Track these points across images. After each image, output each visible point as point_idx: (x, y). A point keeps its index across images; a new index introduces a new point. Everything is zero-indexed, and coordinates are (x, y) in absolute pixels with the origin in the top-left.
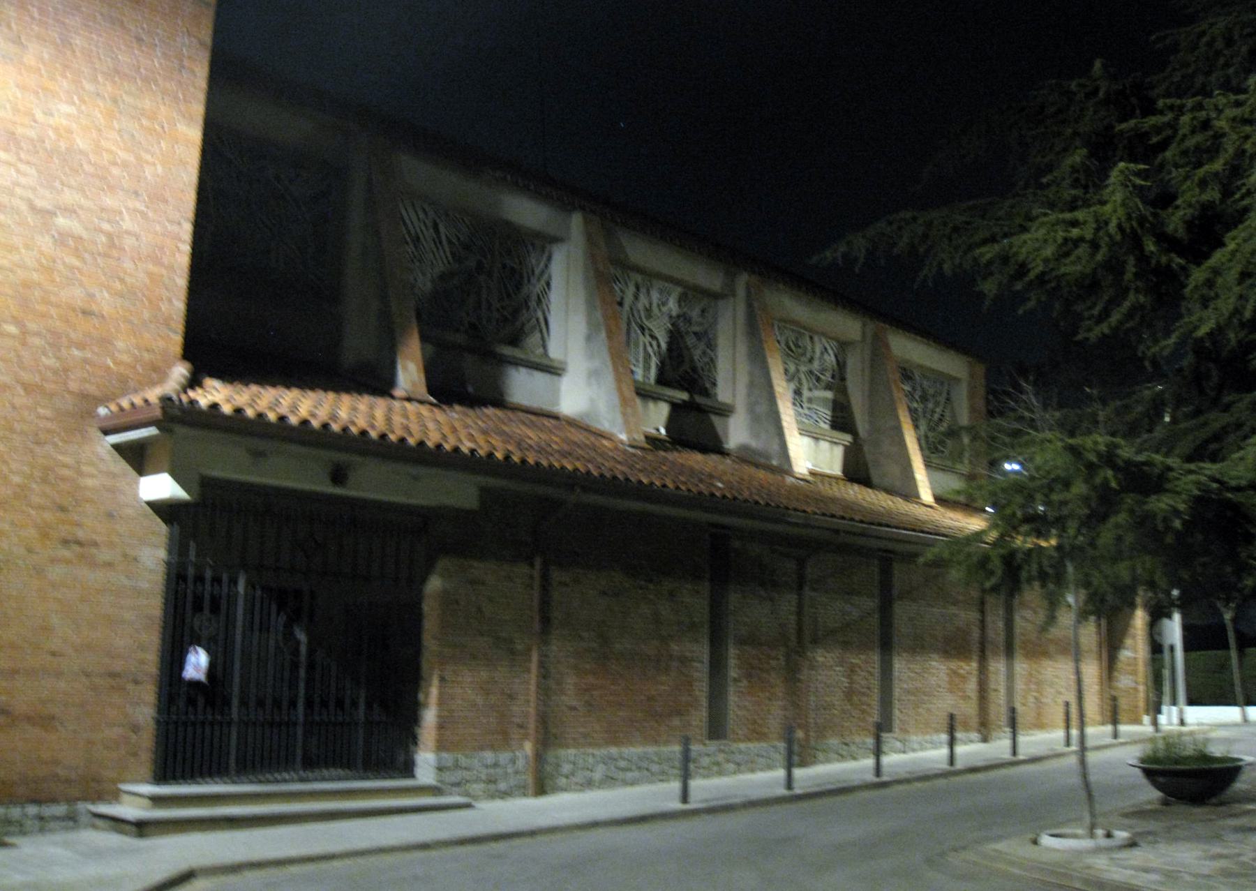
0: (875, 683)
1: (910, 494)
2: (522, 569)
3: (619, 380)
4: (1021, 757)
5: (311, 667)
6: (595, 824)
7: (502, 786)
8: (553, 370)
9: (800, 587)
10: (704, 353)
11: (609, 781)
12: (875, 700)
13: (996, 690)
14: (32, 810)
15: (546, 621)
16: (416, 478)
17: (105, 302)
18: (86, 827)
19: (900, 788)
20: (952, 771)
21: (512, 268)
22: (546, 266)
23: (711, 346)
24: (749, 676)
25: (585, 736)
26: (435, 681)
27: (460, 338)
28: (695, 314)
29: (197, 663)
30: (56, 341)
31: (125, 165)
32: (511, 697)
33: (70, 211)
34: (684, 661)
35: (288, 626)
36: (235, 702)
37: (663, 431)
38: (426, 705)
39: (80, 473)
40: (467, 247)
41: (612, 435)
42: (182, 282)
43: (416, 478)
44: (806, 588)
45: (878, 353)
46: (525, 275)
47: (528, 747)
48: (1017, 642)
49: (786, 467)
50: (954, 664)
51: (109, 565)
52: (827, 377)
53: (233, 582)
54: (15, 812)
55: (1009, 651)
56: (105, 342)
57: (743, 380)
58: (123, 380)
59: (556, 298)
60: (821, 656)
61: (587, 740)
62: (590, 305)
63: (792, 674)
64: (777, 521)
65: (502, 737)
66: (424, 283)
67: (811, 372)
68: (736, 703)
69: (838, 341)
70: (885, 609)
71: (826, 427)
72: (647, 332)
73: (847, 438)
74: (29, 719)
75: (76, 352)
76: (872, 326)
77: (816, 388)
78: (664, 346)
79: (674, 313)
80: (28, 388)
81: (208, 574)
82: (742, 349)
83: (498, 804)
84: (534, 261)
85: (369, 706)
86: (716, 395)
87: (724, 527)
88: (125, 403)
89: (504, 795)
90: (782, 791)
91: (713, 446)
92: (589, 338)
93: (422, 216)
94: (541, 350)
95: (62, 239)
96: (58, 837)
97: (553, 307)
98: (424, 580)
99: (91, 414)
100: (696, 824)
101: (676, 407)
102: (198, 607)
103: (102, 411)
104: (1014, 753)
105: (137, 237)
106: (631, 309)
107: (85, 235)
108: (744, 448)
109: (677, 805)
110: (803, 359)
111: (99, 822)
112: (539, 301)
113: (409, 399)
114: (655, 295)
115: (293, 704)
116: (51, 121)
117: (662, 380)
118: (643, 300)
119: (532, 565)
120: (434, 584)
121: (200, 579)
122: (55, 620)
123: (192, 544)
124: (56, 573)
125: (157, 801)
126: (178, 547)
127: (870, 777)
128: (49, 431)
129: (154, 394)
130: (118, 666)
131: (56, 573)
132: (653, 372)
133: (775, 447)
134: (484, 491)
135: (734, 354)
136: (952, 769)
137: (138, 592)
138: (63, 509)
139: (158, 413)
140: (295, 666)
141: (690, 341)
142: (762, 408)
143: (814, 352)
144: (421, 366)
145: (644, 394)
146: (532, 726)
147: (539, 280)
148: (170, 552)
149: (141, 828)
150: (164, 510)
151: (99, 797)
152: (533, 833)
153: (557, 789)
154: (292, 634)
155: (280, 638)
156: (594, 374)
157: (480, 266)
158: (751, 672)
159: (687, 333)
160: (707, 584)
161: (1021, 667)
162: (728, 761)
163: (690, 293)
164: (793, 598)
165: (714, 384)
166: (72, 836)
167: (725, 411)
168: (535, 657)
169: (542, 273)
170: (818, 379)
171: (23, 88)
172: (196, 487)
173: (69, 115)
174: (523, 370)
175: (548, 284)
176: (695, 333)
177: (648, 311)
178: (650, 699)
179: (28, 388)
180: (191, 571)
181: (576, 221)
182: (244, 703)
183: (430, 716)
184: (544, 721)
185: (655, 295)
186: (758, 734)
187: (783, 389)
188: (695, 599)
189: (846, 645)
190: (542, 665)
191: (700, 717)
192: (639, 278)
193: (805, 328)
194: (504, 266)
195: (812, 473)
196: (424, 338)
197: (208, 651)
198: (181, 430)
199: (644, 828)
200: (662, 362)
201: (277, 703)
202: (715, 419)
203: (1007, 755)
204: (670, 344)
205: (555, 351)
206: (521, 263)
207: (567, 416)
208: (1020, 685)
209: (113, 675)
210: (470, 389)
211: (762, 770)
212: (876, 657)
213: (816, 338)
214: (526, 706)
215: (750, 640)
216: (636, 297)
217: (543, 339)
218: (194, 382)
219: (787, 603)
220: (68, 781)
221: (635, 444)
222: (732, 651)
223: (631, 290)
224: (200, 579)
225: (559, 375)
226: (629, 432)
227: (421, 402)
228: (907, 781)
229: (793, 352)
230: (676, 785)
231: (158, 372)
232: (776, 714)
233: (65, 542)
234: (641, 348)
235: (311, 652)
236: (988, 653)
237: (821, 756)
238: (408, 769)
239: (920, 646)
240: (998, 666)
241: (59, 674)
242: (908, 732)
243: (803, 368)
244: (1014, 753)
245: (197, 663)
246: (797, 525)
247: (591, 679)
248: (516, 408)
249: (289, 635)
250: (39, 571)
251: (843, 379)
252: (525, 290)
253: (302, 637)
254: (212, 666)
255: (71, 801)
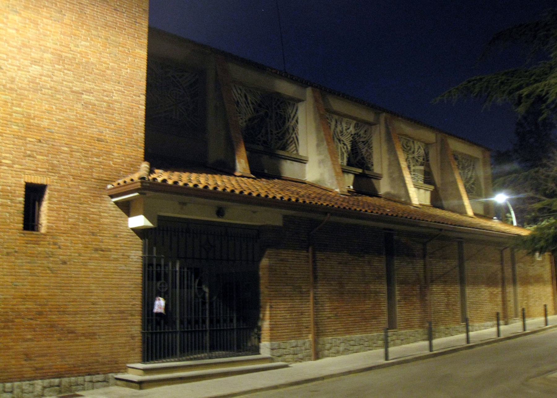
0: (458, 299)
1: (462, 212)
2: (304, 253)
3: (333, 164)
4: (527, 331)
5: (211, 304)
6: (350, 372)
7: (300, 356)
8: (302, 161)
9: (424, 256)
10: (367, 150)
11: (346, 351)
12: (458, 307)
13: (509, 301)
14: (88, 378)
15: (315, 277)
16: (254, 212)
17: (108, 135)
18: (112, 385)
19: (479, 348)
20: (499, 339)
21: (281, 115)
22: (296, 113)
23: (370, 148)
24: (405, 299)
25: (335, 330)
26: (268, 308)
27: (261, 148)
28: (362, 132)
29: (160, 305)
30: (86, 154)
31: (113, 69)
32: (302, 314)
33: (89, 92)
34: (377, 293)
35: (200, 284)
36: (178, 322)
37: (352, 187)
38: (263, 320)
39: (101, 217)
40: (260, 106)
41: (333, 190)
42: (142, 123)
43: (254, 212)
44: (427, 257)
45: (444, 149)
46: (287, 118)
47: (310, 336)
48: (518, 279)
49: (409, 201)
50: (491, 289)
51: (116, 260)
52: (421, 160)
53: (174, 266)
54: (80, 379)
55: (514, 282)
56: (109, 153)
57: (385, 164)
58: (118, 171)
59: (301, 128)
60: (436, 288)
61: (336, 332)
62: (318, 130)
63: (423, 296)
64: (413, 226)
65: (298, 333)
66: (242, 123)
67: (414, 157)
68: (400, 312)
69: (425, 143)
70: (461, 266)
71: (422, 182)
72: (342, 142)
73: (432, 187)
74: (83, 335)
75: (95, 159)
76: (439, 136)
77: (417, 165)
78: (349, 148)
79: (353, 133)
80: (75, 177)
81: (162, 262)
82: (385, 147)
83: (298, 365)
84: (290, 111)
85: (238, 320)
86: (373, 170)
87: (390, 230)
88: (121, 182)
89: (301, 360)
90: (427, 352)
91: (374, 193)
92: (318, 145)
93: (239, 92)
94: (295, 152)
95: (86, 105)
96: (101, 390)
97: (299, 132)
98: (260, 260)
99: (104, 188)
100: (395, 370)
101: (357, 176)
102: (158, 279)
103: (109, 186)
104: (524, 330)
105: (121, 103)
106: (334, 131)
107: (96, 102)
108: (388, 193)
109: (383, 361)
110: (410, 152)
111: (119, 382)
112: (294, 130)
113: (242, 176)
114: (344, 125)
115: (204, 322)
116: (79, 50)
117: (349, 164)
118: (339, 128)
119: (308, 251)
120: (265, 262)
121: (159, 265)
122: (93, 287)
123: (155, 249)
124: (92, 265)
125: (147, 371)
126: (148, 250)
127: (464, 344)
128: (86, 197)
129: (136, 177)
130: (123, 307)
131: (92, 265)
132: (345, 160)
133: (403, 192)
134: (285, 217)
135: (381, 151)
136: (499, 338)
137: (131, 272)
138: (93, 234)
139: (139, 185)
140: (204, 303)
141: (361, 145)
142: (396, 175)
143: (414, 149)
144: (247, 161)
145: (344, 171)
146: (312, 326)
147: (293, 119)
148: (144, 252)
149: (141, 384)
150: (140, 232)
151: (118, 371)
152: (323, 378)
153: (324, 356)
154: (201, 289)
155: (197, 291)
156: (321, 162)
157: (266, 114)
158: (406, 297)
159: (359, 142)
160: (384, 256)
161: (520, 289)
162: (398, 339)
163: (360, 123)
164: (422, 262)
165: (372, 165)
166: (107, 390)
167: (378, 177)
168: (312, 295)
169: (294, 117)
170: (417, 161)
171: (64, 34)
172: (156, 221)
173: (86, 47)
174: (289, 161)
175: (297, 121)
176: (363, 142)
177: (341, 132)
178: (363, 311)
179: (75, 177)
180: (155, 263)
181: (309, 92)
182: (182, 323)
183: (266, 325)
184: (316, 324)
185: (344, 125)
186: (409, 325)
187: (404, 165)
188: (379, 263)
189: (445, 282)
190: (315, 298)
191: (384, 319)
192: (336, 117)
193: (410, 138)
194: (277, 113)
195: (420, 205)
196: (247, 149)
197: (165, 299)
198: (150, 194)
199: (372, 373)
200: (349, 155)
201: (197, 322)
202: (374, 181)
203: (520, 330)
204: (352, 147)
205: (302, 152)
206: (284, 112)
207: (309, 182)
208: (519, 298)
209: (122, 312)
210: (266, 171)
211: (412, 343)
212: (458, 288)
213: (415, 142)
214: (308, 319)
215: (403, 282)
216: (336, 126)
217: (296, 146)
218: (151, 172)
219: (419, 264)
220: (104, 364)
221: (344, 193)
222: (397, 288)
223: (333, 123)
224: (159, 265)
225: (305, 163)
226: (340, 188)
227: (249, 178)
228: (482, 345)
229: (406, 149)
230: (382, 351)
231: (135, 168)
232: (417, 315)
233: (96, 250)
234: (339, 150)
235: (211, 297)
236: (506, 284)
237: (437, 335)
238: (256, 350)
239: (476, 282)
240: (510, 289)
241: (96, 313)
242: (474, 322)
243: (410, 156)
244: (524, 330)
245: (160, 305)
246: (425, 227)
247: (336, 304)
248: (286, 179)
249: (200, 290)
250: (85, 264)
251: (428, 161)
252: (287, 124)
253: (207, 290)
254: (166, 306)
255: (105, 373)
